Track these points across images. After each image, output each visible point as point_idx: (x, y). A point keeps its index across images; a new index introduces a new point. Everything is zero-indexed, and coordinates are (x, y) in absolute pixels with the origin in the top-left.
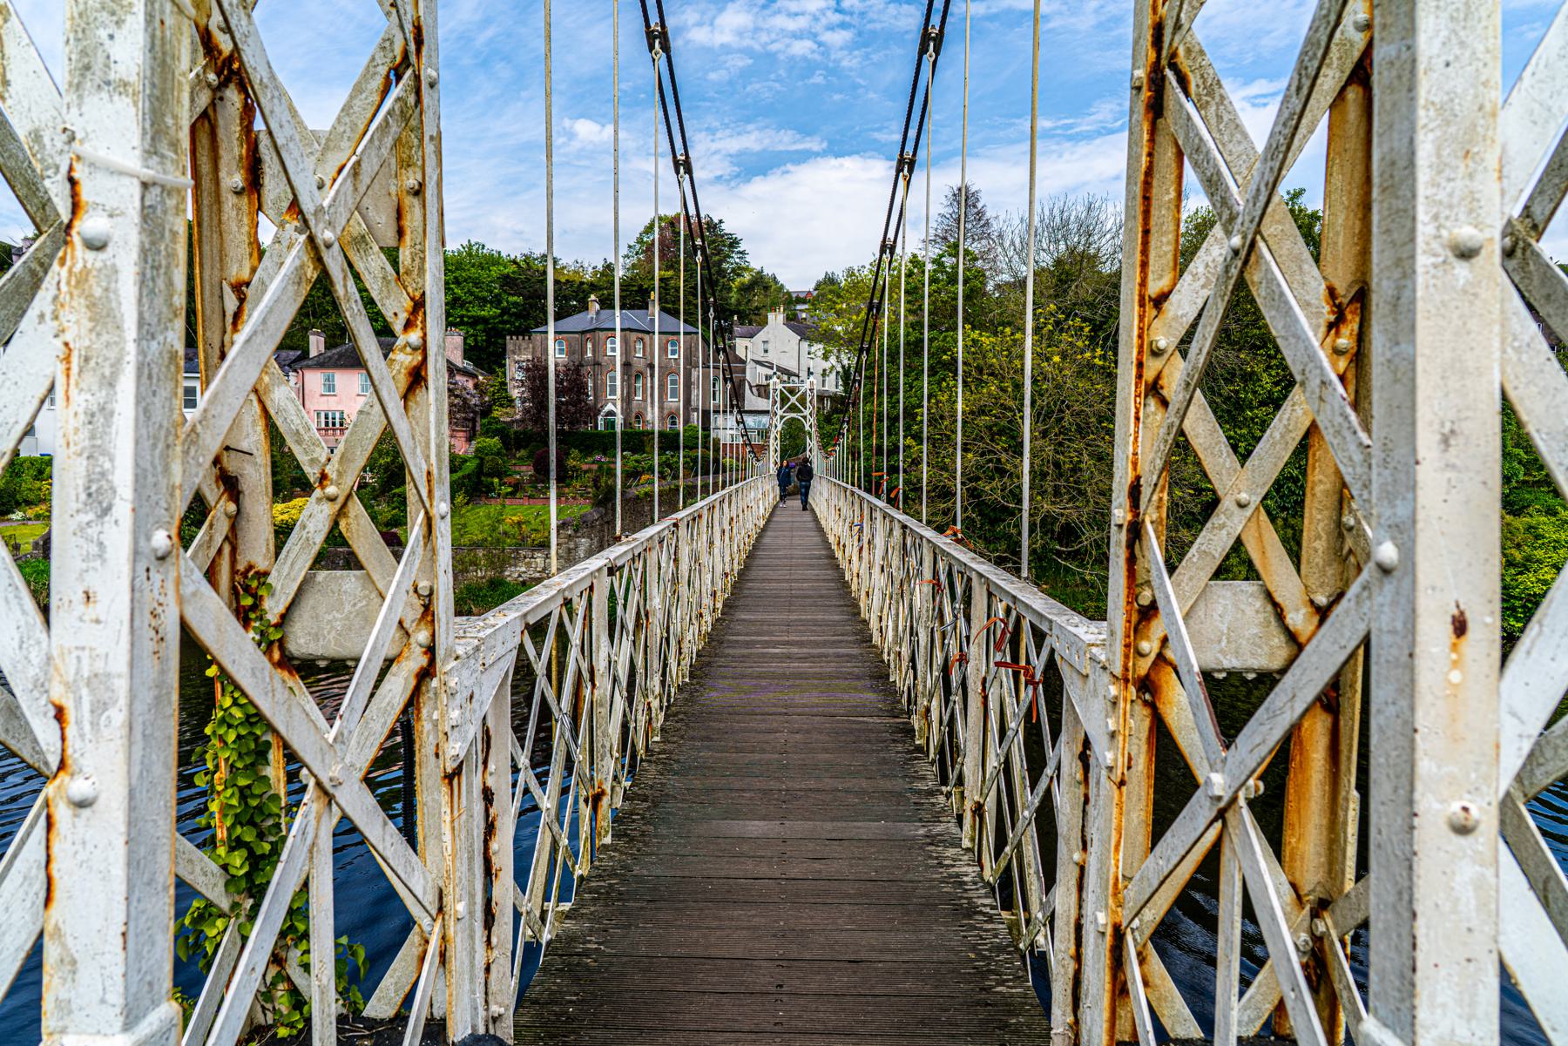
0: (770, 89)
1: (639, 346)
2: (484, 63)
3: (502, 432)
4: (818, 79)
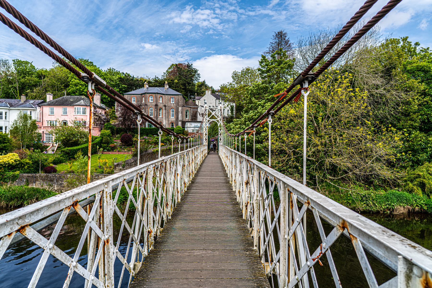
0: (198, 35)
1: (161, 99)
2: (117, 28)
3: (112, 129)
4: (211, 32)
